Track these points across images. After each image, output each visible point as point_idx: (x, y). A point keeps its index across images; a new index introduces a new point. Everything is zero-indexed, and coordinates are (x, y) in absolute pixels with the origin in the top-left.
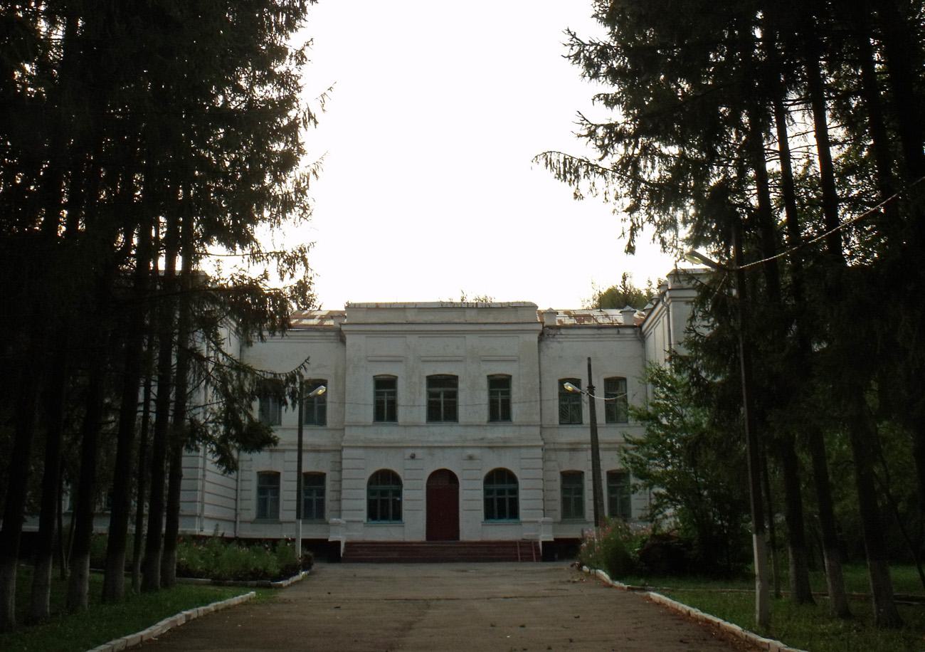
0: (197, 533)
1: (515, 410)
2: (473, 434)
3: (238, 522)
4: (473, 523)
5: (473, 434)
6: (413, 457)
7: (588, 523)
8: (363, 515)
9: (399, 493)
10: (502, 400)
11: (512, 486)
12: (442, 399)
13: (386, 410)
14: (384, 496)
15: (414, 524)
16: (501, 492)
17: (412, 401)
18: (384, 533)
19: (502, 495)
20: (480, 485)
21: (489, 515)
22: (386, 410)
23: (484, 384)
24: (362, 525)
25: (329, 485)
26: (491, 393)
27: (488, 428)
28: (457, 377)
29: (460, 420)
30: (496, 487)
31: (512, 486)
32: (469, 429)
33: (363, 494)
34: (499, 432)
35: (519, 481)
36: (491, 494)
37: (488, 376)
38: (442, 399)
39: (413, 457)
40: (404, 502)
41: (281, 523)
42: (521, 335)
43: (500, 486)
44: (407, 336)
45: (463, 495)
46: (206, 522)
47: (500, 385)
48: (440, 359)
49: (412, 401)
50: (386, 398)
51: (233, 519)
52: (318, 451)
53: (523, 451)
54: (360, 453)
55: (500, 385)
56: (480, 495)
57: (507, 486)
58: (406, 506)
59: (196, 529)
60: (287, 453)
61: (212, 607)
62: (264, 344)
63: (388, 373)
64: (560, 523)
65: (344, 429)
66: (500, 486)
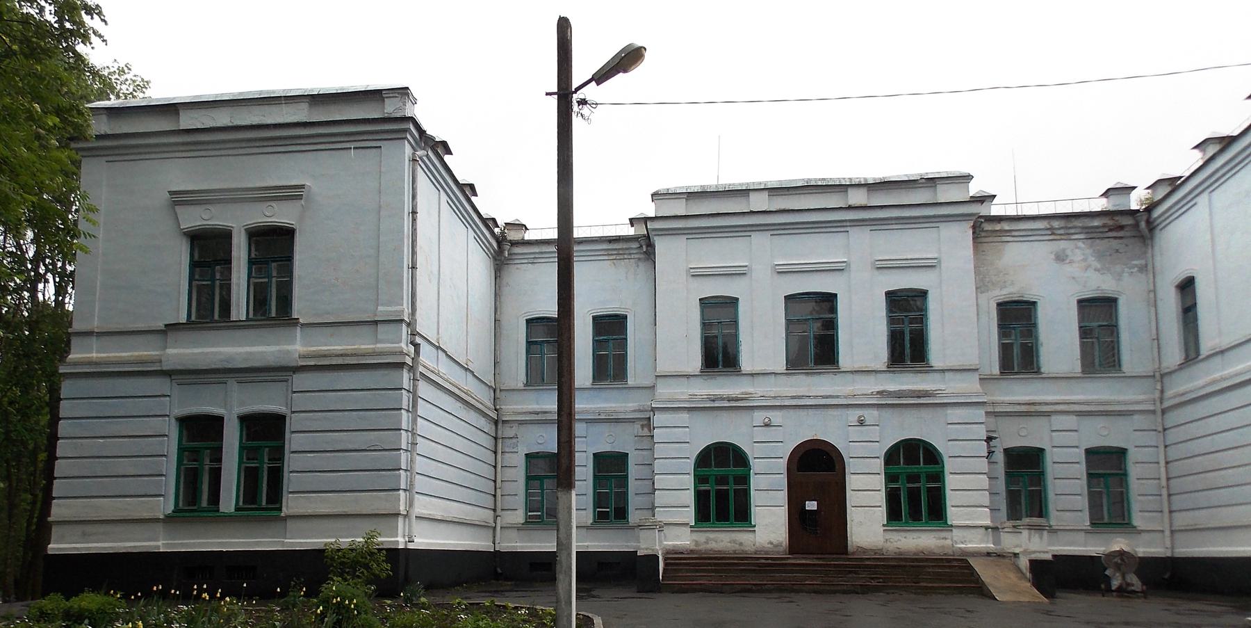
0: (401, 546)
3: (498, 528)
4: (867, 523)
5: (868, 386)
8: (689, 515)
9: (744, 480)
11: (740, 471)
12: (815, 334)
13: (720, 355)
14: (722, 483)
15: (769, 525)
16: (722, 480)
17: (763, 340)
18: (723, 540)
19: (916, 482)
20: (879, 465)
21: (894, 514)
22: (720, 355)
25: (633, 471)
26: (891, 321)
28: (737, 299)
30: (715, 471)
31: (740, 471)
35: (946, 459)
38: (815, 334)
39: (861, 423)
40: (948, 493)
41: (633, 528)
43: (722, 471)
46: (418, 527)
47: (907, 310)
49: (763, 340)
56: (879, 482)
57: (732, 470)
58: (756, 497)
59: (400, 539)
60: (1053, 418)
62: (853, 266)
64: (587, 528)
65: (653, 387)
66: (722, 471)
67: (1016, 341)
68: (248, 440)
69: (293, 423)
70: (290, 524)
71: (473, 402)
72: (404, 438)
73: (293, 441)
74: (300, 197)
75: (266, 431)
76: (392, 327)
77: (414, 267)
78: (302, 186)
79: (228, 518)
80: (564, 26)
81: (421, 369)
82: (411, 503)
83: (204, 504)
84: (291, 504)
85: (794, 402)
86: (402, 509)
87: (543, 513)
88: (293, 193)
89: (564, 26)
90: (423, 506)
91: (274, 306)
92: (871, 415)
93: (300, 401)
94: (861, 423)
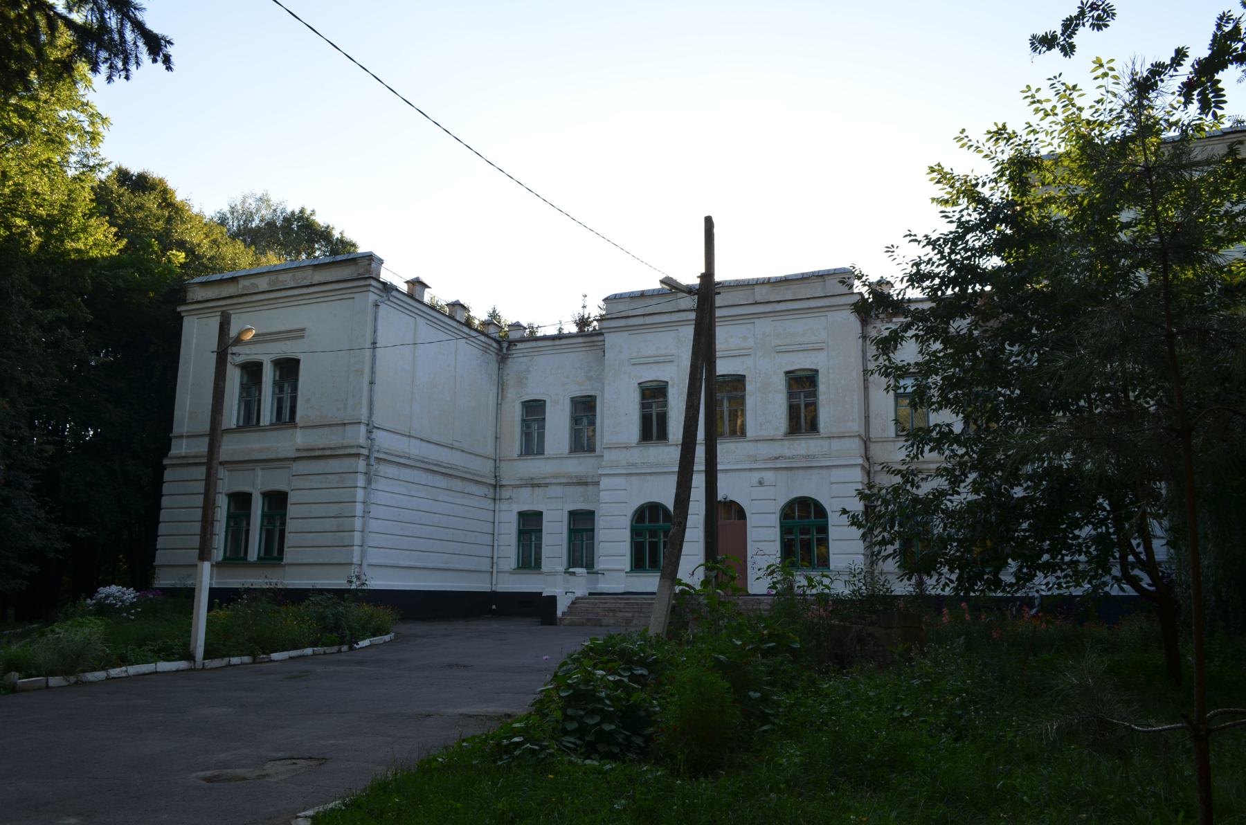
1: (825, 416)
2: (765, 450)
5: (765, 450)
6: (761, 483)
7: (553, 574)
8: (626, 563)
10: (658, 415)
23: (780, 383)
24: (623, 574)
26: (791, 395)
27: (786, 443)
29: (821, 430)
32: (759, 445)
33: (626, 535)
34: (803, 446)
35: (748, 515)
36: (808, 533)
37: (787, 373)
41: (597, 573)
42: (829, 314)
44: (756, 321)
45: (752, 534)
47: (802, 384)
48: (810, 347)
50: (655, 410)
51: (488, 568)
52: (586, 484)
53: (835, 472)
54: (621, 481)
55: (802, 384)
56: (775, 534)
61: (115, 672)
63: (808, 367)
67: (802, 401)
68: (269, 508)
69: (292, 498)
70: (287, 569)
71: (465, 475)
72: (359, 509)
73: (292, 511)
74: (303, 337)
75: (277, 501)
76: (356, 426)
77: (372, 383)
78: (303, 330)
79: (253, 565)
80: (709, 222)
81: (376, 455)
82: (363, 555)
83: (276, 554)
84: (289, 556)
85: (423, 465)
86: (356, 560)
87: (529, 559)
88: (298, 334)
89: (709, 222)
90: (374, 557)
91: (286, 416)
92: (769, 476)
93: (296, 483)
94: (761, 483)
